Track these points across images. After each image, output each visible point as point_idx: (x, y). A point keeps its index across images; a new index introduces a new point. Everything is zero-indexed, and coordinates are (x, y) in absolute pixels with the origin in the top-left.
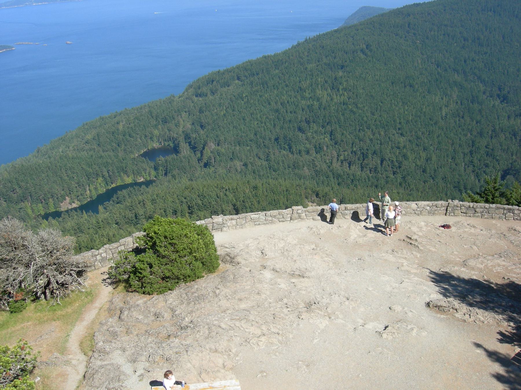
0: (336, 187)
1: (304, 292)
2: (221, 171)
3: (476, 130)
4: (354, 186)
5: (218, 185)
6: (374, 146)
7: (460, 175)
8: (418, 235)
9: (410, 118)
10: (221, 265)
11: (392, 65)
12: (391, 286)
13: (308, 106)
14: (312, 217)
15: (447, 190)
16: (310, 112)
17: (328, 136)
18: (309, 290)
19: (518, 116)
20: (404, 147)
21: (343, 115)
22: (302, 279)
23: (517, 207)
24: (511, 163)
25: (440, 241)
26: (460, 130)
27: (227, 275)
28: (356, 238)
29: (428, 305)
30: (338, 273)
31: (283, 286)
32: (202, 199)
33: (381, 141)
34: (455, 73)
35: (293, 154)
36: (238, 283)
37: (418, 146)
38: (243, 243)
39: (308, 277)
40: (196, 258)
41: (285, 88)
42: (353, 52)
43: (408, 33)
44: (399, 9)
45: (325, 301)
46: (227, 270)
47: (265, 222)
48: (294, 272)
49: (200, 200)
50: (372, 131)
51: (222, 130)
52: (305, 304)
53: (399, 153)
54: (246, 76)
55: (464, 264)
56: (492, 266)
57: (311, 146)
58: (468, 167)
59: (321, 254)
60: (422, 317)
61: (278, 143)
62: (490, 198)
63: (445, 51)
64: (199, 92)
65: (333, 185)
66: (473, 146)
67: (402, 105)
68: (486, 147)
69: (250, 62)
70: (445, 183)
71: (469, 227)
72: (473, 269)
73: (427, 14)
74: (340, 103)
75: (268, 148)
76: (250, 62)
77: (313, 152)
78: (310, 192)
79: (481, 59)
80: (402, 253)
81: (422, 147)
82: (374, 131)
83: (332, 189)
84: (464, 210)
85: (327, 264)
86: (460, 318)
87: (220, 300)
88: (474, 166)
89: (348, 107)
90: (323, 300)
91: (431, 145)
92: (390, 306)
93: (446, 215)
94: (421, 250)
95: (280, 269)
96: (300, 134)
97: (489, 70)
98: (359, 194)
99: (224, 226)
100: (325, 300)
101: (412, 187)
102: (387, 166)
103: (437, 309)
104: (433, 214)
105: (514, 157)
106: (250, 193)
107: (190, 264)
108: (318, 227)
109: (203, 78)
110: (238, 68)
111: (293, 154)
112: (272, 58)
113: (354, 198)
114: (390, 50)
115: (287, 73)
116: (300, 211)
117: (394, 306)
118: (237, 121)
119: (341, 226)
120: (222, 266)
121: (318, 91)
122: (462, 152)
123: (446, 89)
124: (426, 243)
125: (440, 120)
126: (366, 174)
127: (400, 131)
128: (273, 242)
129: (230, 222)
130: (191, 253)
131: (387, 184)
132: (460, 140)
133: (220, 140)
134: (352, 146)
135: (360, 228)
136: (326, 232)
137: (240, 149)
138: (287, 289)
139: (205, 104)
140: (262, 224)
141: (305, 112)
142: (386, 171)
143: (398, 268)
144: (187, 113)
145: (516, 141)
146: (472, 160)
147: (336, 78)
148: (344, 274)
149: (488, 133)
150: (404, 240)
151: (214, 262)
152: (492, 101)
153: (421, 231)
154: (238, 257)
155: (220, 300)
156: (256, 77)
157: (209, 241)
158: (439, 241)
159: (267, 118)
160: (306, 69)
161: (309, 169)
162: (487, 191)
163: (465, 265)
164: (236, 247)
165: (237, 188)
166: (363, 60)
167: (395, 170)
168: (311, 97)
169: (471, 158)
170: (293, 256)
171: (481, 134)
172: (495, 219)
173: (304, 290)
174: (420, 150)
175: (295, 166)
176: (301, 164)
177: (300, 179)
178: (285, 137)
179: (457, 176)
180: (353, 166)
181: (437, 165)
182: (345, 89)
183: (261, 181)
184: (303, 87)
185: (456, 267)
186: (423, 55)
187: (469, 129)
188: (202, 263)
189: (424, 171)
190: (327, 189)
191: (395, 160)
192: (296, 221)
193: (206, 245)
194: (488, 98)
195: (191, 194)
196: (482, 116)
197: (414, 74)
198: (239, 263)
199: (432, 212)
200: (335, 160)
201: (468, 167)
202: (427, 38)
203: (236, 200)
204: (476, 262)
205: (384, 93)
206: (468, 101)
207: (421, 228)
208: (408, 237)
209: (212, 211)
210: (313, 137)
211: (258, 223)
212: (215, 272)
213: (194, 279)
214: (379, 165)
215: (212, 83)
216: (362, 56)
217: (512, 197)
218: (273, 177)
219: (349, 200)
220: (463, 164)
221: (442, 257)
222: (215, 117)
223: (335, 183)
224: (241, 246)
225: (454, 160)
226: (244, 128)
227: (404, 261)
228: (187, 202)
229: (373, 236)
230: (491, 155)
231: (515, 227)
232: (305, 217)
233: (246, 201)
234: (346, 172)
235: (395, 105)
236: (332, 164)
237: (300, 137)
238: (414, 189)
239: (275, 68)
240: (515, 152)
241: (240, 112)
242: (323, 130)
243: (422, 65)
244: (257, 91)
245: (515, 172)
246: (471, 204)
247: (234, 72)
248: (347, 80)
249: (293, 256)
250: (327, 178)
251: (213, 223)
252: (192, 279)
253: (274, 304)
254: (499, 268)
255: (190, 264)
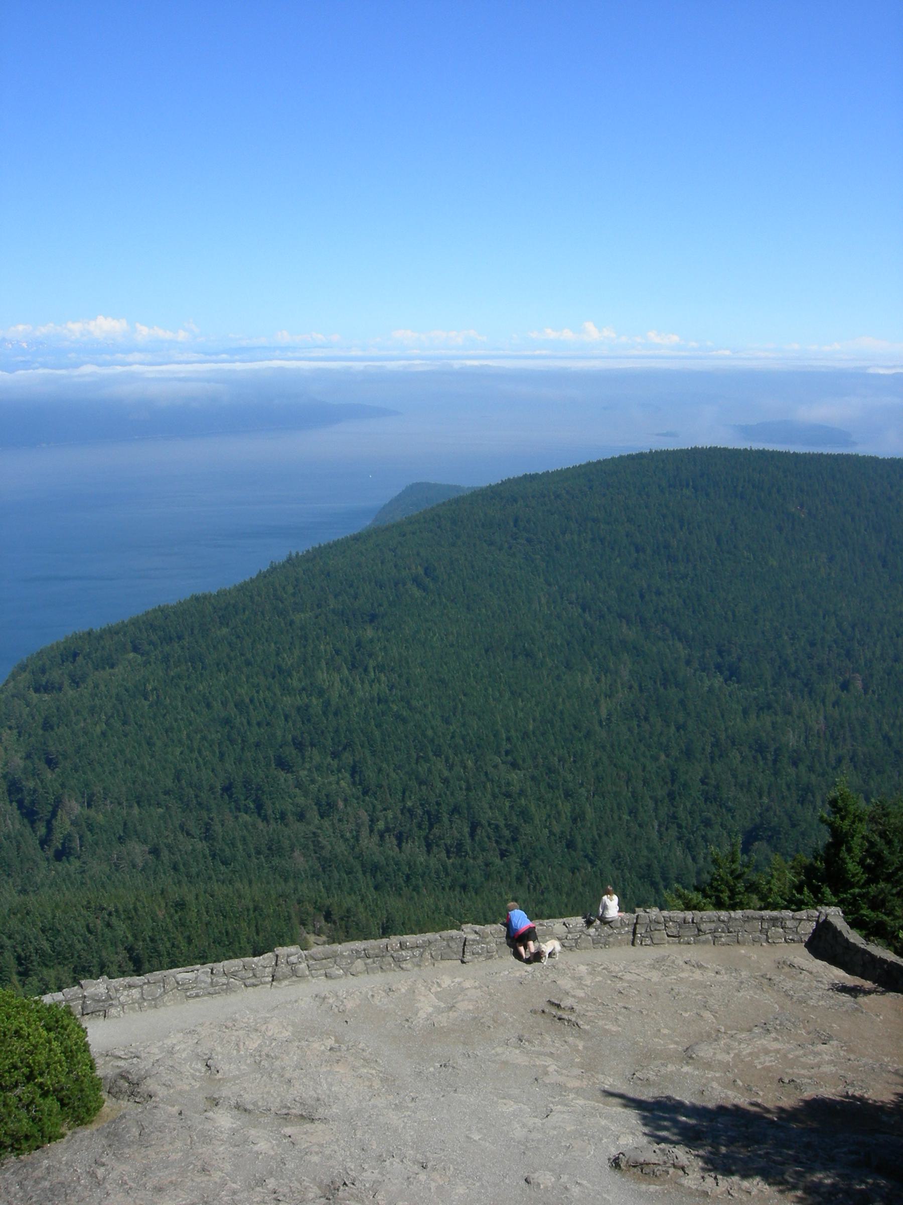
0: (371, 894)
1: (315, 1159)
2: (98, 868)
3: (678, 745)
4: (414, 890)
5: (89, 902)
6: (452, 794)
7: (651, 850)
8: (574, 996)
9: (531, 727)
10: (105, 1104)
11: (484, 610)
12: (524, 1125)
13: (299, 709)
14: (322, 972)
15: (624, 884)
16: (303, 723)
17: (347, 775)
18: (328, 1152)
19: (765, 710)
20: (522, 792)
21: (378, 726)
22: (308, 1126)
23: (789, 913)
24: (760, 815)
25: (627, 1006)
26: (642, 748)
27: (123, 1129)
28: (431, 1014)
29: (616, 1163)
30: (396, 1105)
31: (262, 1146)
32: (52, 938)
33: (467, 782)
34: (621, 621)
35: (268, 822)
36: (151, 1145)
37: (552, 788)
38: (161, 1043)
39: (324, 1120)
40: (43, 1089)
41: (245, 670)
42: (396, 584)
43: (515, 539)
44: (494, 487)
45: (370, 1175)
46: (123, 1117)
47: (211, 990)
48: (289, 1108)
49: (47, 940)
50: (447, 761)
51: (99, 769)
52: (320, 1188)
53: (512, 807)
54: (151, 643)
55: (688, 1055)
56: (750, 1054)
57: (310, 801)
58: (667, 829)
59: (351, 1059)
60: (605, 1196)
61: (230, 797)
62: (725, 896)
63: (597, 577)
64: (44, 680)
65: (363, 890)
66: (673, 781)
67: (510, 699)
68: (703, 782)
69: (162, 611)
70: (618, 869)
71: (688, 967)
72: (708, 1066)
73: (553, 497)
74: (372, 700)
75: (209, 810)
76: (162, 611)
77: (313, 814)
78: (311, 910)
79: (676, 588)
80: (541, 1043)
81: (561, 791)
82: (451, 761)
83: (362, 900)
84: (673, 929)
85: (367, 1083)
86: (694, 1187)
87: (108, 1194)
88: (680, 826)
89: (389, 706)
90: (364, 1174)
91: (582, 785)
92: (526, 1175)
93: (633, 944)
94: (585, 1032)
95: (255, 1104)
96: (282, 775)
97: (694, 612)
98: (426, 909)
99: (111, 1005)
100: (369, 1173)
101: (544, 884)
102: (486, 839)
103: (637, 1171)
104: (605, 944)
105: (765, 800)
106: (168, 920)
107: (28, 1106)
108: (340, 994)
109: (52, 648)
110: (133, 624)
111: (268, 822)
112: (213, 601)
113: (414, 918)
114: (478, 577)
115: (248, 635)
116: (293, 959)
117: (536, 1175)
118: (134, 747)
119: (394, 988)
120: (109, 1105)
121: (319, 673)
122: (651, 797)
123: (605, 657)
124: (594, 1014)
125: (598, 728)
126: (439, 860)
127: (509, 758)
128: (233, 1038)
129: (126, 993)
130: (30, 1078)
131: (487, 880)
132: (644, 770)
133: (93, 795)
134: (403, 797)
135: (439, 989)
136: (358, 1006)
137: (140, 813)
138: (273, 1153)
139: (58, 709)
140: (204, 995)
141: (290, 724)
142: (483, 850)
143: (536, 1079)
144: (15, 731)
145: (766, 764)
146: (674, 813)
147: (359, 644)
148: (410, 1105)
149: (703, 749)
150: (543, 1012)
151: (88, 1096)
152: (705, 678)
153: (581, 986)
154: (149, 1081)
155: (108, 1194)
156: (176, 645)
157: (76, 1044)
158: (625, 1008)
159: (204, 738)
160: (291, 625)
161: (304, 855)
162: (717, 880)
163: (691, 1058)
164: (143, 1055)
165: (136, 909)
166: (419, 601)
167: (504, 846)
168: (304, 689)
169: (672, 809)
170: (283, 1068)
171: (688, 754)
172: (744, 944)
173: (317, 1153)
174: (557, 798)
175: (274, 849)
176: (286, 843)
177: (286, 880)
178: (247, 783)
179: (645, 852)
180: (407, 842)
181: (597, 829)
182: (380, 668)
183: (192, 888)
184: (287, 664)
185: (669, 1066)
186: (550, 585)
187: (661, 744)
188: (61, 1100)
189: (571, 845)
190: (349, 901)
191: (502, 823)
192: (286, 982)
193: (69, 1054)
194: (698, 673)
195: (25, 926)
196: (688, 714)
197: (532, 628)
198: (151, 1097)
199: (603, 941)
200: (365, 832)
201: (667, 829)
202: (557, 548)
203: (135, 936)
204: (714, 1049)
205: (469, 674)
206: (655, 682)
207: (581, 978)
208: (551, 1003)
209: (76, 967)
210: (311, 780)
211: (193, 992)
212: (91, 1122)
213: (39, 1143)
214: (467, 835)
215: (75, 660)
216: (417, 593)
217: (770, 889)
218: (221, 877)
219: (403, 924)
220: (656, 824)
221: (636, 1043)
222: (82, 740)
223: (368, 885)
224: (156, 1051)
225: (635, 816)
226: (150, 764)
227: (549, 1061)
228: (14, 947)
229: (471, 1007)
230: (715, 799)
231: (792, 958)
232: (307, 973)
233: (158, 937)
234: (393, 859)
235: (494, 699)
236: (358, 840)
237: (282, 780)
238: (551, 888)
239: (221, 623)
240: (766, 788)
241: (141, 726)
242: (335, 764)
243: (549, 608)
244: (180, 677)
245: (770, 834)
246: (689, 915)
247: (125, 634)
248: (385, 647)
249: (283, 1068)
250: (348, 873)
251: (85, 997)
252: (34, 1145)
253: (245, 1195)
254: (767, 1059)
255: (28, 1106)
